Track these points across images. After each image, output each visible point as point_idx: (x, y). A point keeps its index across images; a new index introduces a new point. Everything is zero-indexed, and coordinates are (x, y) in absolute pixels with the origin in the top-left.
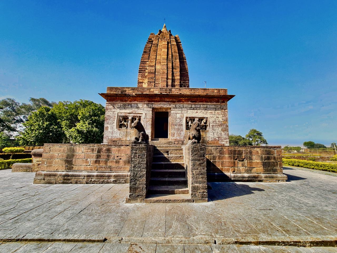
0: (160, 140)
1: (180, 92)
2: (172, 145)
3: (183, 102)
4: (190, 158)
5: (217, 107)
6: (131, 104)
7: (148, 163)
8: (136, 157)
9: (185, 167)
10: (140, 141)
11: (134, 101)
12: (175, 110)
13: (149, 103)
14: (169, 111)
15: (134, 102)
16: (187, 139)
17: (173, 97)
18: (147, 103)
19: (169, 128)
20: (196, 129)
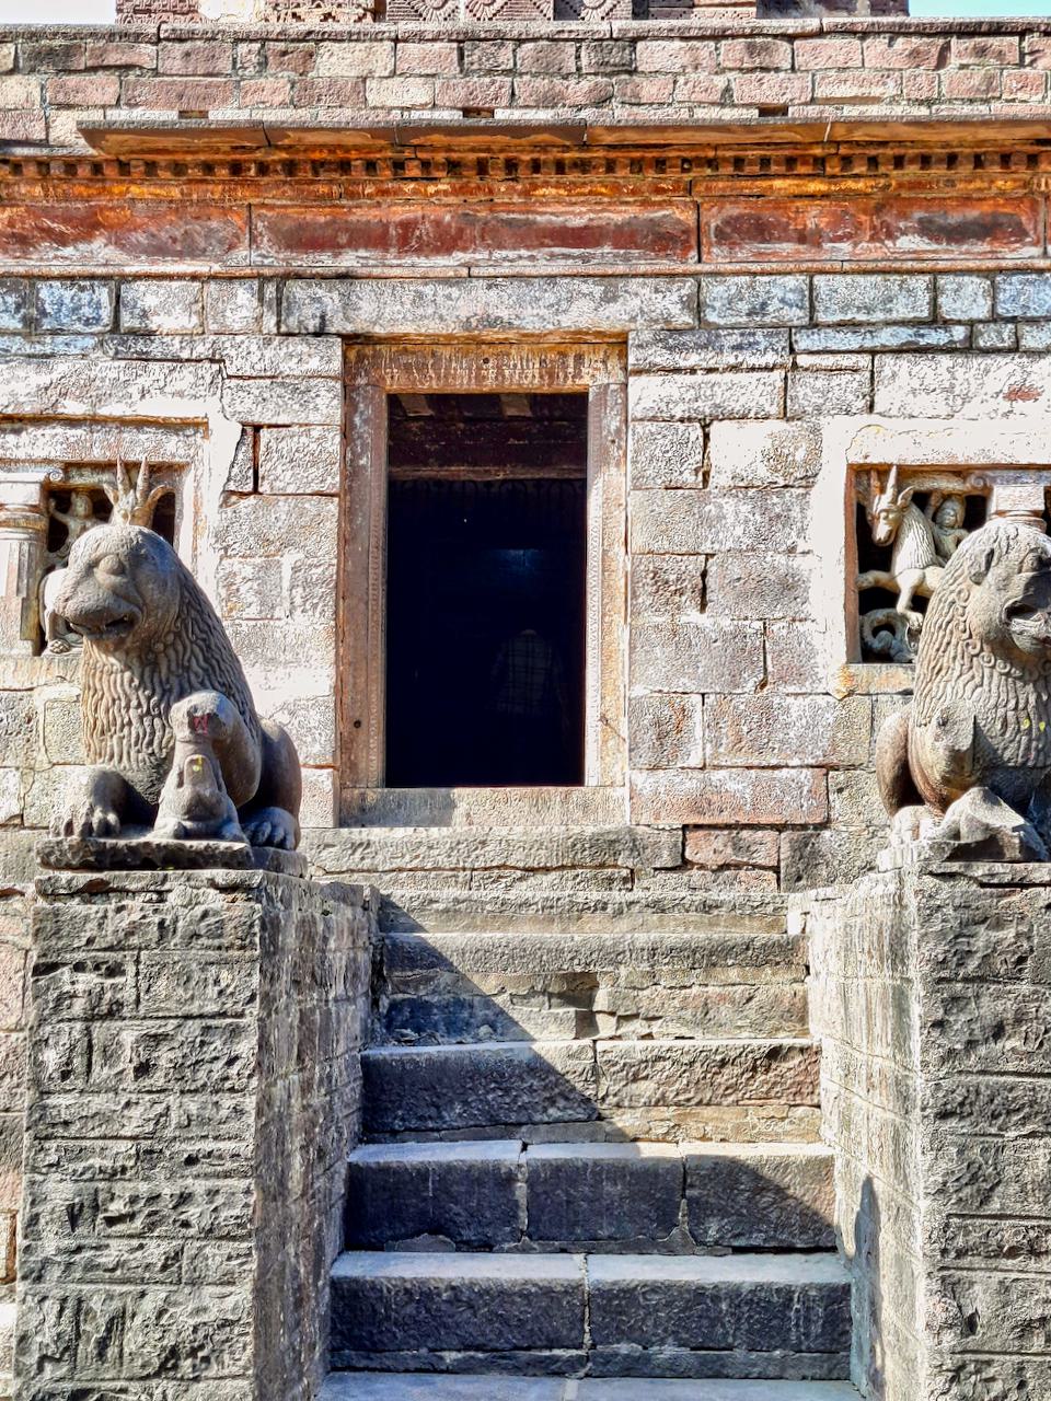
0: (458, 814)
1: (770, 90)
2: (637, 894)
4: (920, 1084)
6: (33, 279)
7: (286, 1156)
8: (101, 1073)
9: (842, 1212)
10: (163, 831)
11: (62, 240)
12: (693, 359)
13: (304, 261)
14: (593, 377)
15: (68, 251)
16: (875, 796)
18: (273, 258)
19: (604, 633)
20: (1000, 643)
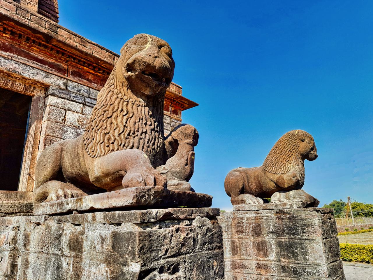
3: (88, 80)
17: (63, 54)
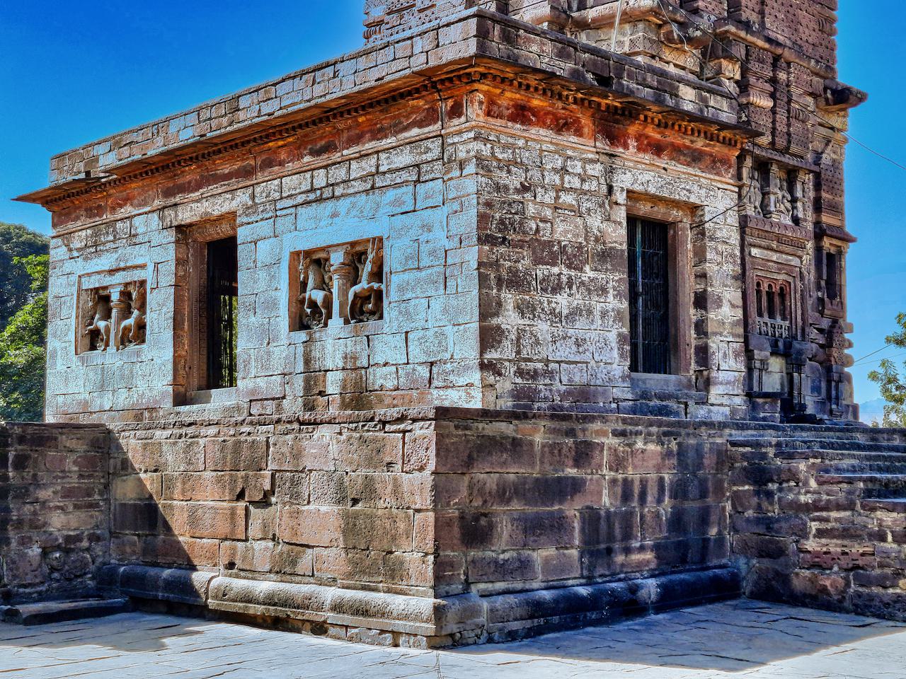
5: (424, 157)
